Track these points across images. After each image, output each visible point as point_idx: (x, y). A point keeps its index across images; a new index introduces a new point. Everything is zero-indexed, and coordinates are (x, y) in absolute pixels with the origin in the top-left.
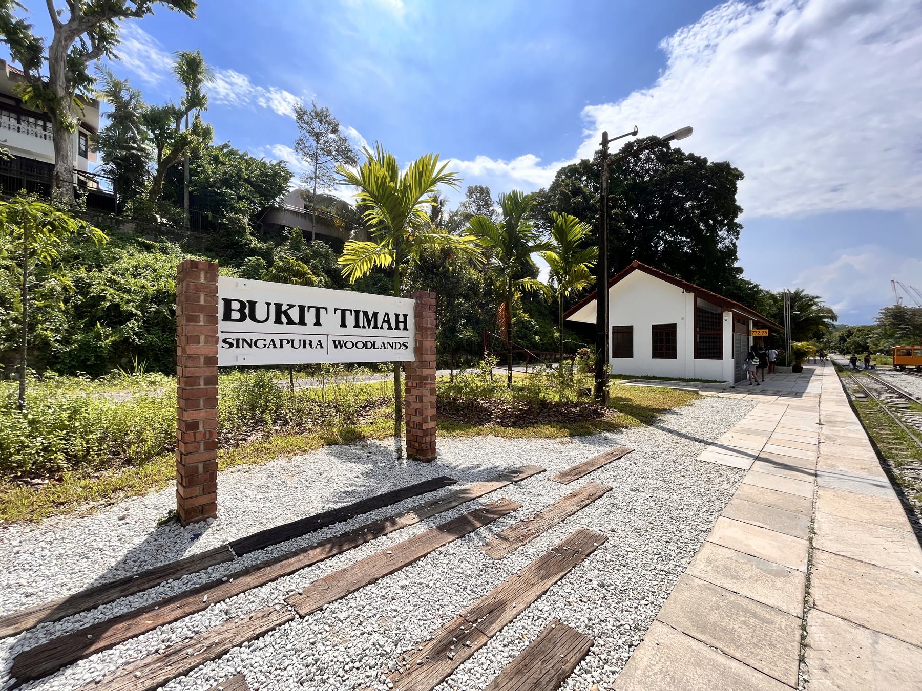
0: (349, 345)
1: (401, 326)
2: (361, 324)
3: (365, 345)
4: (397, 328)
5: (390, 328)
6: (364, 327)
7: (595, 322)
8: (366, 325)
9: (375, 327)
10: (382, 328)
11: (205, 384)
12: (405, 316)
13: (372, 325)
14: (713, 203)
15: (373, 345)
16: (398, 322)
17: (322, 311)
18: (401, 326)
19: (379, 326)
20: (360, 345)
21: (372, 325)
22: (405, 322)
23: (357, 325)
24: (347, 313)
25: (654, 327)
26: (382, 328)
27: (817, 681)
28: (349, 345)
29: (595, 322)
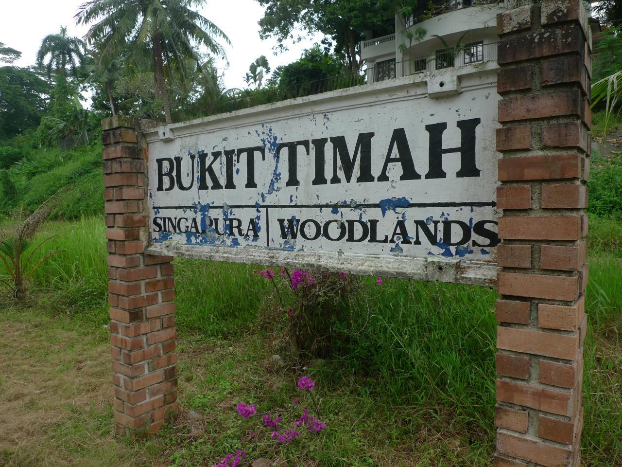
0: (310, 230)
1: (451, 163)
2: (328, 174)
3: (347, 231)
4: (436, 171)
5: (409, 173)
6: (336, 180)
7: (246, 153)
8: (341, 174)
9: (366, 176)
10: (383, 177)
11: (150, 397)
12: (468, 127)
13: (356, 172)
14: (167, 54)
15: (370, 231)
16: (436, 151)
17: (257, 155)
18: (451, 163)
19: (376, 172)
20: (334, 231)
21: (356, 172)
22: (467, 150)
23: (320, 179)
24: (301, 149)
25: (403, 129)
26: (383, 177)
27: (11, 329)
28: (310, 230)
29: (246, 153)
